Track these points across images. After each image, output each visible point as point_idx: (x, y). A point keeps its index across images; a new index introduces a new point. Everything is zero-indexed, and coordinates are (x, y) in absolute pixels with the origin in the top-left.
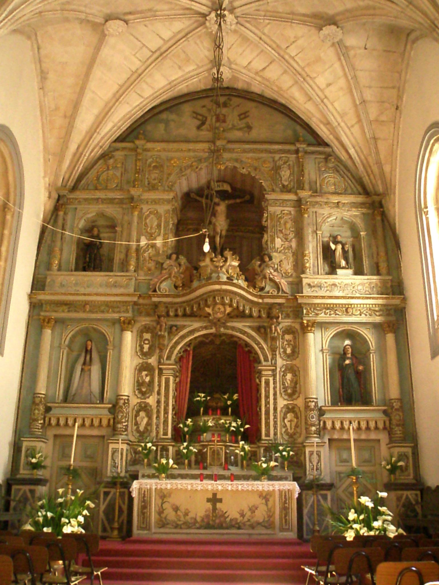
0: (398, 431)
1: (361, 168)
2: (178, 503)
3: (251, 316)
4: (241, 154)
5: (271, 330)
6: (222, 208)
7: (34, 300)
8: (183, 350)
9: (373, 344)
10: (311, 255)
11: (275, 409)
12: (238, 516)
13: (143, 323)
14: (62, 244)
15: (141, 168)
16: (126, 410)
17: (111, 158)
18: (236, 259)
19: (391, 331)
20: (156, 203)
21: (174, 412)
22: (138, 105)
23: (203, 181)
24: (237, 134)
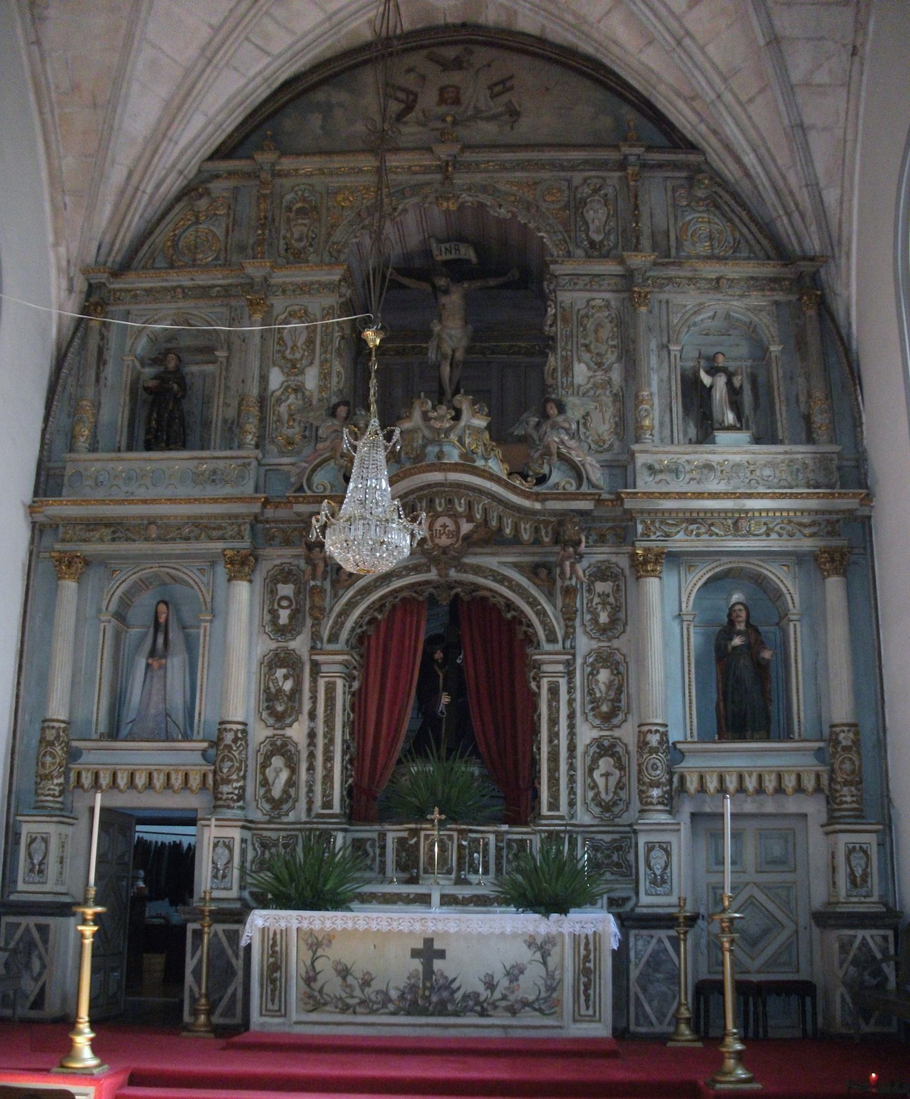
0: (847, 795)
1: (770, 197)
2: (347, 960)
3: (516, 540)
4: (496, 175)
5: (563, 573)
6: (454, 300)
7: (40, 518)
8: (367, 618)
9: (796, 598)
10: (656, 400)
11: (572, 748)
12: (481, 988)
13: (278, 562)
14: (98, 394)
15: (269, 214)
16: (240, 753)
17: (201, 196)
18: (480, 411)
19: (836, 572)
20: (303, 292)
21: (347, 758)
22: (260, 72)
23: (414, 241)
24: (488, 130)
